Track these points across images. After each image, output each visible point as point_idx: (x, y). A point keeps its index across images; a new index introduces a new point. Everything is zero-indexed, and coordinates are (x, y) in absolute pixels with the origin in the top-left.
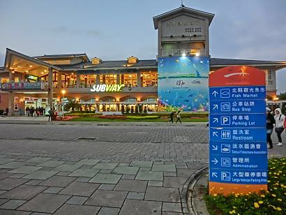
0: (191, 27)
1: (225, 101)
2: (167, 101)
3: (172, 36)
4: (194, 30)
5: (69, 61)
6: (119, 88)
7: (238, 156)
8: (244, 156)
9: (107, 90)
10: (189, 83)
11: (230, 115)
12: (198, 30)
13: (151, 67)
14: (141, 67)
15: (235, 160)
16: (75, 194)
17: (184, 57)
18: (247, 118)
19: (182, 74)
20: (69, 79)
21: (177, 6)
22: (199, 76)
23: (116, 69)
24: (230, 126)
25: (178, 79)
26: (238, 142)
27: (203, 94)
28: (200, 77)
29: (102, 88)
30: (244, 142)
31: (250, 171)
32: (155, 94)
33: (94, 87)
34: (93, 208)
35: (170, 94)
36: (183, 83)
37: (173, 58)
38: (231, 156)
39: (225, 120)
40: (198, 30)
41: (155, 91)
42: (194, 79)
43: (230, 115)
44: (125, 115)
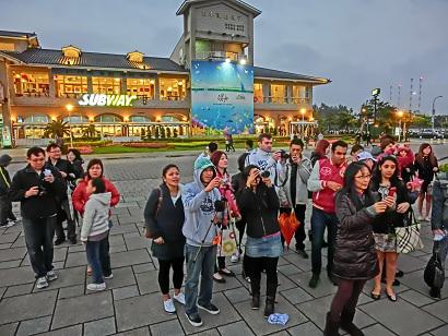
0: (232, 22)
3: (209, 33)
5: (12, 45)
6: (129, 100)
9: (109, 104)
10: (232, 97)
12: (240, 28)
14: (159, 68)
16: (414, 308)
17: (226, 66)
19: (226, 86)
20: (18, 80)
23: (89, 69)
25: (220, 93)
27: (247, 112)
29: (99, 100)
32: (187, 111)
33: (85, 97)
34: (64, 324)
35: (207, 112)
37: (212, 64)
40: (240, 28)
41: (187, 106)
42: (238, 93)
44: (83, 139)
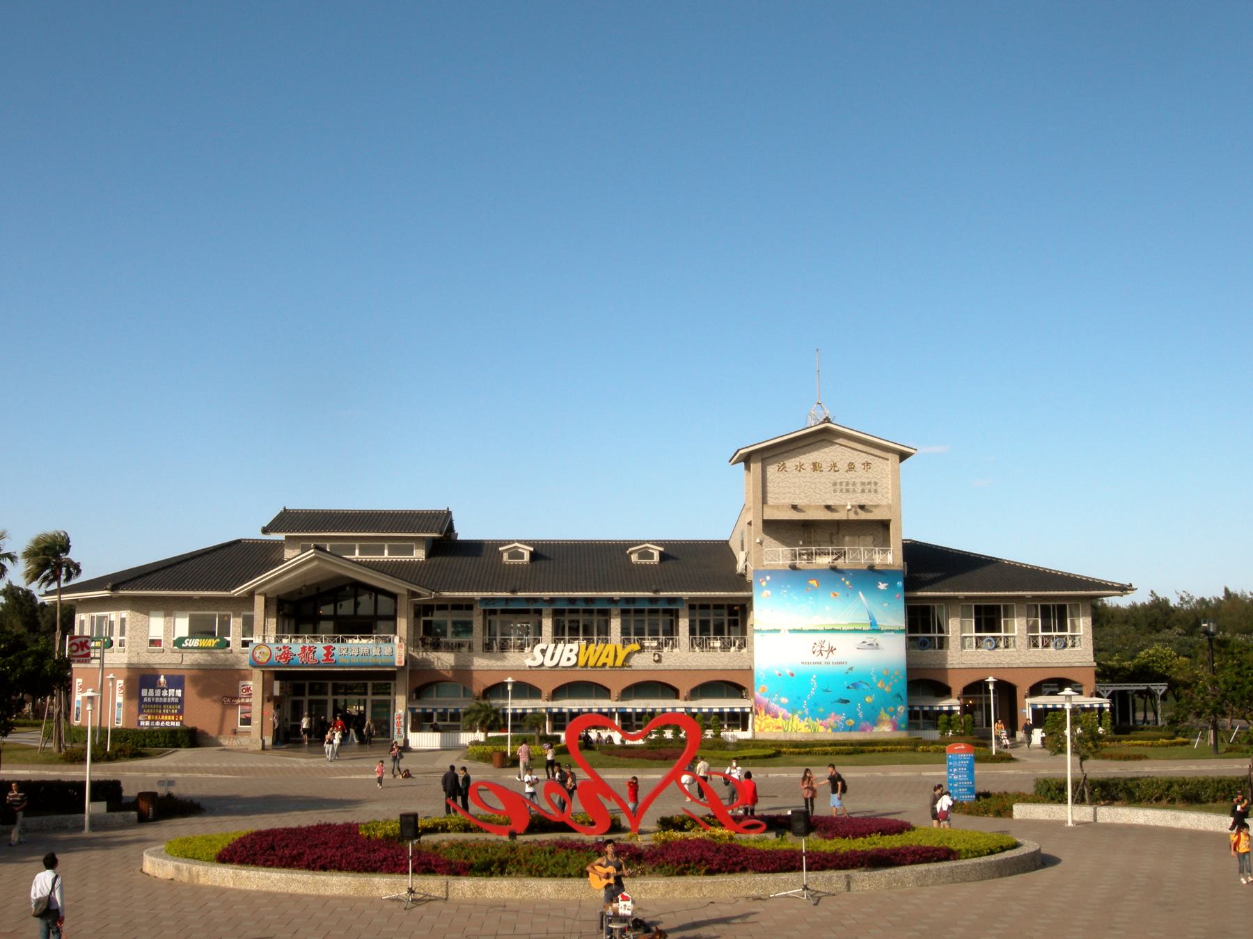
1: (955, 760)
2: (784, 700)
4: (859, 488)
7: (962, 788)
8: (964, 788)
11: (957, 767)
13: (1235, 850)
15: (960, 790)
18: (965, 769)
21: (813, 425)
22: (875, 629)
24: (957, 774)
26: (961, 781)
28: (879, 631)
30: (964, 781)
31: (967, 795)
36: (832, 650)
38: (958, 788)
39: (955, 770)
43: (957, 767)
